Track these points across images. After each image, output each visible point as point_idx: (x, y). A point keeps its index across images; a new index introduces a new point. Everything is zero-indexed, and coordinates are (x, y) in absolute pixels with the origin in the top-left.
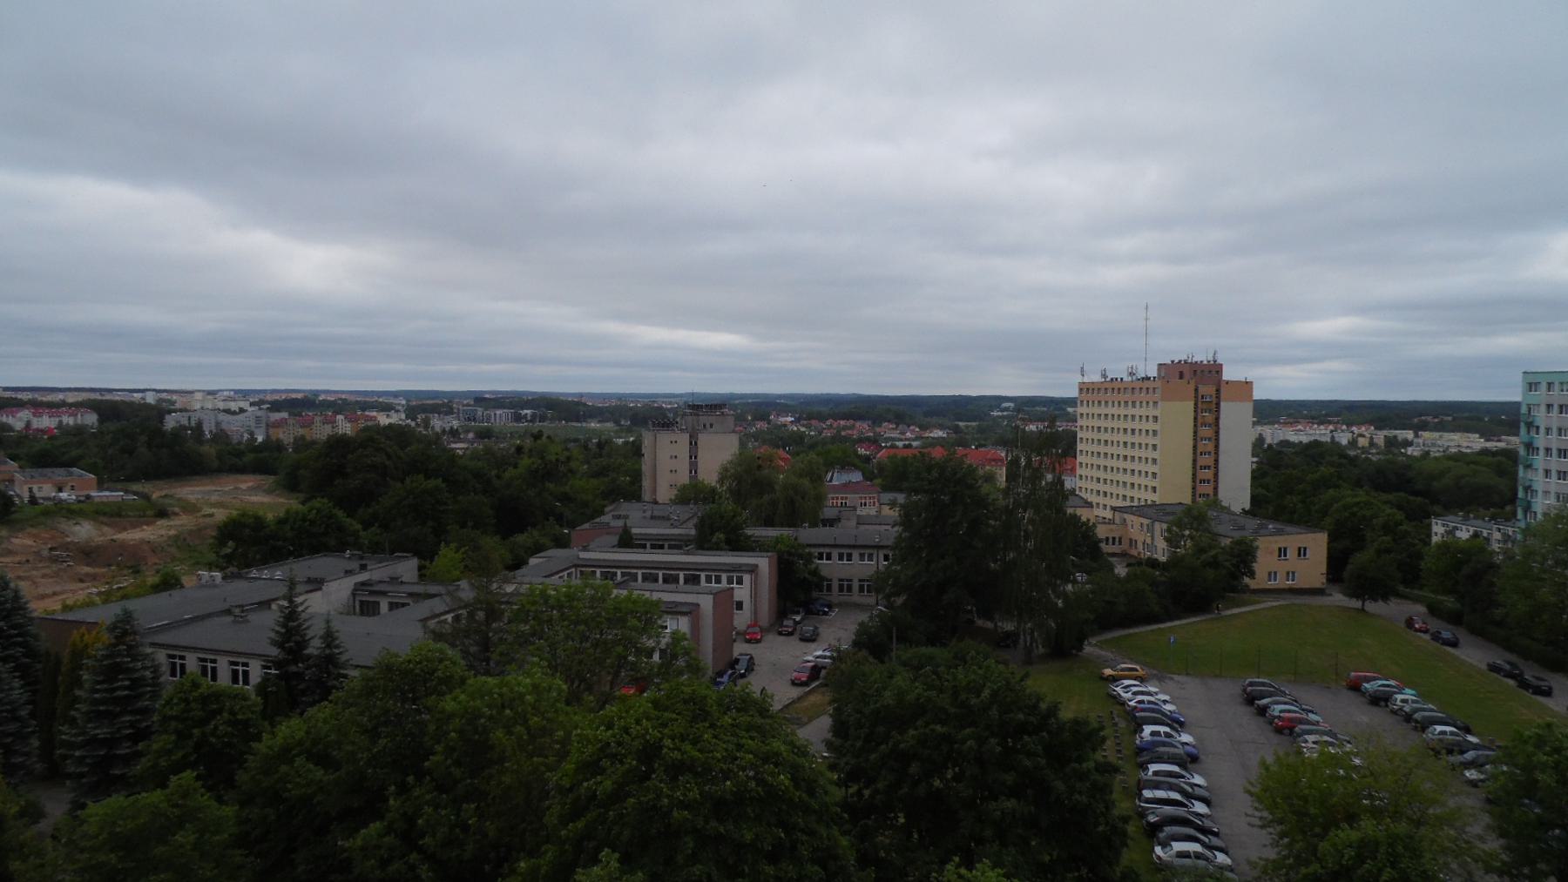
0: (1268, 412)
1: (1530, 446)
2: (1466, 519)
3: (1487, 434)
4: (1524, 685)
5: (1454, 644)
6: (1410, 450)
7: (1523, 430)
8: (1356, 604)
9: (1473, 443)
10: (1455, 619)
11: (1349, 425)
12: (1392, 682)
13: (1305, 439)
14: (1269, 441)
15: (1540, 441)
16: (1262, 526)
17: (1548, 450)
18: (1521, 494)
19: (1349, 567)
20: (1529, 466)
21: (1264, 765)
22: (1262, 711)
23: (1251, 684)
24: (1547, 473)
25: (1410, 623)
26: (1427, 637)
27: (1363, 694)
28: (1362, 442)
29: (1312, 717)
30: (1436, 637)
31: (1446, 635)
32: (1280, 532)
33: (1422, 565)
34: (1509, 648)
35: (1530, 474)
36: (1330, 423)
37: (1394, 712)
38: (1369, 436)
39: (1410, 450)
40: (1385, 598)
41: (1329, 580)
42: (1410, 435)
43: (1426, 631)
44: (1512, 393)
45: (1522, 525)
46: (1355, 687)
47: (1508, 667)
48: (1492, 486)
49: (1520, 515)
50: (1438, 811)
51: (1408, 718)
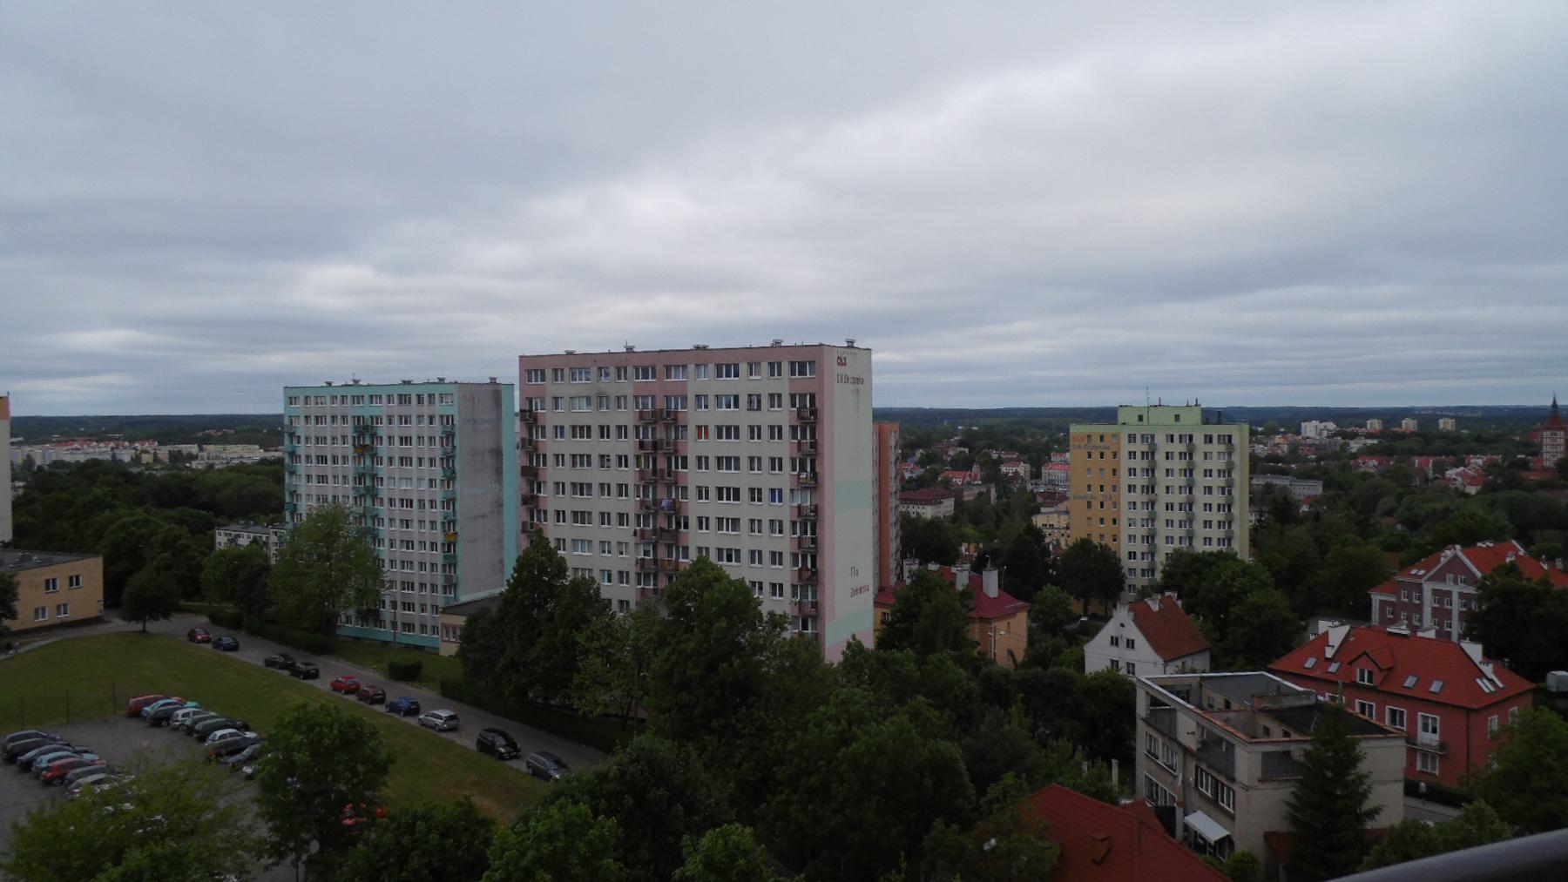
0: (33, 430)
1: (293, 455)
2: (247, 526)
3: (266, 446)
4: (296, 673)
5: (234, 648)
6: (194, 464)
7: (287, 440)
8: (139, 626)
9: (254, 453)
10: (235, 624)
11: (131, 441)
12: (174, 700)
13: (82, 458)
14: (38, 462)
15: (302, 450)
16: (24, 559)
17: (308, 457)
18: (288, 499)
19: (127, 589)
20: (292, 473)
21: (15, 826)
22: (27, 767)
23: (13, 740)
24: (309, 477)
25: (192, 636)
26: (209, 646)
27: (144, 718)
28: (146, 458)
29: (87, 757)
30: (218, 645)
31: (226, 640)
32: (48, 563)
33: (202, 576)
34: (282, 639)
35: (295, 481)
36: (111, 439)
37: (176, 729)
38: (154, 453)
39: (194, 464)
40: (166, 616)
41: (106, 607)
42: (194, 449)
43: (208, 641)
44: (275, 407)
45: (290, 526)
46: (135, 713)
47: (282, 660)
48: (262, 496)
49: (288, 518)
50: (210, 816)
51: (190, 731)
